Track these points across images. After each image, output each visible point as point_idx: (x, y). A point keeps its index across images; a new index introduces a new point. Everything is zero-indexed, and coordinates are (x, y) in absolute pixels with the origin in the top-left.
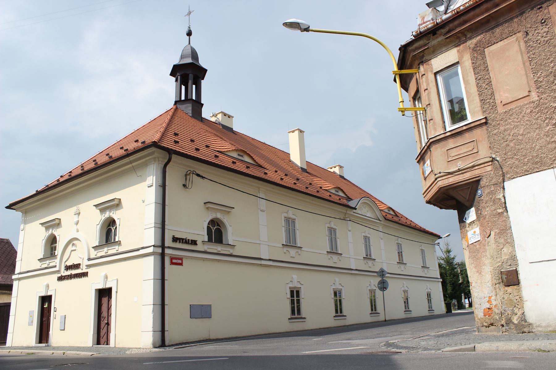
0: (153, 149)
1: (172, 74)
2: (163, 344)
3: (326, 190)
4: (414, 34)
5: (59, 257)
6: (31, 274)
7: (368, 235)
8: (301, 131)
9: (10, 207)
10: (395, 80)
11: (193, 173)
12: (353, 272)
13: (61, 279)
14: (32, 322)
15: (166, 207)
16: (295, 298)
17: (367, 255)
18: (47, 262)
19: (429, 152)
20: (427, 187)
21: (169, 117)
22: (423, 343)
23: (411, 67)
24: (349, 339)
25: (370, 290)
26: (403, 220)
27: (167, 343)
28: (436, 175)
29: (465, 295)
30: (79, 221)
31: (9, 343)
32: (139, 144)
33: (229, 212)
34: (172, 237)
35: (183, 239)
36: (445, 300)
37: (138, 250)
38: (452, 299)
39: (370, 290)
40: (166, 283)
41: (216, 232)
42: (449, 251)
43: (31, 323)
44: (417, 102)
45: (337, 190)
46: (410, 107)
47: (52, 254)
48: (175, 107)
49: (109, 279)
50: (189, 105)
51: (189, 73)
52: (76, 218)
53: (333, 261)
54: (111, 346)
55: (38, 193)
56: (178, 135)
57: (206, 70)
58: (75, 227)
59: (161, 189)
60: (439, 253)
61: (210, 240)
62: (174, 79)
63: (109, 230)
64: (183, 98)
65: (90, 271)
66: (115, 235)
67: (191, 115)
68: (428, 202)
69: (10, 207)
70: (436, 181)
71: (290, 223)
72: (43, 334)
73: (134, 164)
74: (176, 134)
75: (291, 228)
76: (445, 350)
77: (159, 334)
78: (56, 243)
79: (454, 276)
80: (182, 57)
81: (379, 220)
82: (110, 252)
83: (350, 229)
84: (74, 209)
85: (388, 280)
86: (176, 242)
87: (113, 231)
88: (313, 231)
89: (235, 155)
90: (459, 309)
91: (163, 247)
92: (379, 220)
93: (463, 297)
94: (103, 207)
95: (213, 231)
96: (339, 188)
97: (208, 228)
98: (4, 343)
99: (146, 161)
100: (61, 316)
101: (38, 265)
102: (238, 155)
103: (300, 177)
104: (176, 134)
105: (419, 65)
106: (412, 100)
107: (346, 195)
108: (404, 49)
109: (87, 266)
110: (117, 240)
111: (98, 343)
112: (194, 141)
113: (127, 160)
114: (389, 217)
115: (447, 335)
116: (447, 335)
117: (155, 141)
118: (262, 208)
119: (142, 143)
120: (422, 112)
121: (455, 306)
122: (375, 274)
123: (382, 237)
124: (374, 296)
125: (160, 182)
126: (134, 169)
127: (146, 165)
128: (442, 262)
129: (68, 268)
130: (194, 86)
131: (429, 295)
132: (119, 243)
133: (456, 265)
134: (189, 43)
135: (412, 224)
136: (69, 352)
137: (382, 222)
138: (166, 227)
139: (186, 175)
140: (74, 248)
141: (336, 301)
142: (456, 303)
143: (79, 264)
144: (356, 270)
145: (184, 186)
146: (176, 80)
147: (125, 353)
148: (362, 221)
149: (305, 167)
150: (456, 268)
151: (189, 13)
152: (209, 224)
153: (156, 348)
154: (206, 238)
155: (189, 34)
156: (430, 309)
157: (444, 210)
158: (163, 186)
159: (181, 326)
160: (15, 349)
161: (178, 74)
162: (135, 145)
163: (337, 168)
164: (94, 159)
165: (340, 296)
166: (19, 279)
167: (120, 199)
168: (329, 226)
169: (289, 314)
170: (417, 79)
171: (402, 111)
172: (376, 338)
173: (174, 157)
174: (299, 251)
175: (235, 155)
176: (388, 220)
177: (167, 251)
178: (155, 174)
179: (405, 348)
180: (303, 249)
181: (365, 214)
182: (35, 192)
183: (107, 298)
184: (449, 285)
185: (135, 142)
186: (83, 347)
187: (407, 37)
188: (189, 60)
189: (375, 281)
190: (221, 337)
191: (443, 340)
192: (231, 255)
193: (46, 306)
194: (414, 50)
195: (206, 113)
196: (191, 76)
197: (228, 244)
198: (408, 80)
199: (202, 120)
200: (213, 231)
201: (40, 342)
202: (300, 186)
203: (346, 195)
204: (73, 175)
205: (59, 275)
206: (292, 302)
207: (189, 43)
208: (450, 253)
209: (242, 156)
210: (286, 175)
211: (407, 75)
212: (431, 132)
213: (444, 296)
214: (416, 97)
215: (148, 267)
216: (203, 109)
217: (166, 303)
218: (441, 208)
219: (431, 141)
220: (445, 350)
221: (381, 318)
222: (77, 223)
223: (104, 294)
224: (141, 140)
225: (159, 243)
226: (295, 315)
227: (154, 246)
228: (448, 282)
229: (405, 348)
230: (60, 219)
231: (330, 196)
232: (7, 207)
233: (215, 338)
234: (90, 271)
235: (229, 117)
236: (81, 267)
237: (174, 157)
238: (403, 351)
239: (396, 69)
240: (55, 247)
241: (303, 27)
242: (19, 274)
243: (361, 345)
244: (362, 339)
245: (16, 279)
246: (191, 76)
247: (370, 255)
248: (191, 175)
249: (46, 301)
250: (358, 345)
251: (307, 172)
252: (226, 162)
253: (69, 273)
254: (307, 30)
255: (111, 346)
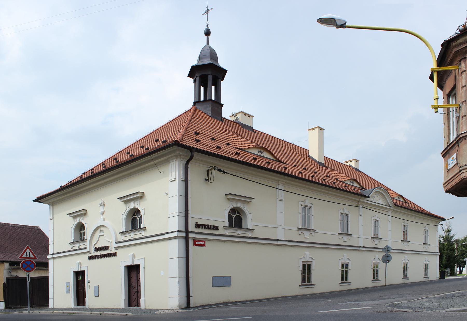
0: (175, 148)
1: (190, 75)
2: (188, 306)
3: (342, 181)
4: (461, 28)
5: (88, 241)
6: (61, 254)
7: (378, 219)
8: (321, 129)
9: (38, 200)
10: (431, 78)
11: (215, 169)
12: (361, 249)
13: (91, 258)
14: (69, 290)
15: (189, 199)
16: (307, 270)
17: (374, 235)
18: (78, 245)
19: (457, 147)
20: (449, 178)
21: (189, 118)
22: (427, 304)
23: (450, 64)
24: (357, 301)
25: (374, 263)
26: (411, 206)
27: (192, 305)
28: (461, 167)
29: (457, 265)
30: (105, 211)
31: (51, 305)
32: (160, 143)
33: (249, 202)
34: (195, 224)
35: (205, 225)
36: (440, 269)
37: (163, 234)
38: (446, 268)
39: (374, 263)
40: (191, 280)
41: (236, 218)
42: (449, 231)
43: (68, 291)
44: (451, 99)
45: (352, 181)
46: (442, 104)
47: (81, 239)
48: (194, 108)
49: (136, 258)
50: (208, 105)
51: (208, 74)
52: (101, 209)
53: (344, 240)
54: (141, 308)
55: (62, 188)
56: (199, 134)
57: (226, 71)
58: (102, 217)
59: (183, 184)
60: (441, 232)
61: (231, 225)
62: (192, 80)
63: (134, 220)
64: (202, 99)
65: (118, 251)
66: (140, 223)
67: (210, 115)
68: (447, 191)
69: (38, 200)
70: (460, 173)
71: (306, 209)
72: (80, 298)
73: (156, 161)
74: (197, 134)
75: (306, 214)
76: (449, 310)
77: (185, 300)
78: (84, 229)
79: (451, 250)
80: (201, 57)
81: (390, 206)
82: (136, 237)
83: (361, 214)
84: (99, 202)
85: (391, 254)
86: (199, 227)
87: (138, 219)
88: (327, 216)
89: (255, 152)
90: (451, 275)
91: (187, 232)
92: (390, 206)
93: (456, 267)
94: (126, 200)
95: (234, 218)
96: (355, 180)
97: (229, 215)
98: (48, 306)
99: (168, 158)
100: (95, 287)
101: (70, 247)
102: (259, 151)
103: (317, 170)
104: (197, 134)
105: (460, 61)
106: (446, 97)
107: (361, 186)
108: (447, 45)
109: (115, 248)
110: (142, 227)
111: (130, 305)
112: (215, 140)
113: (149, 158)
114: (399, 203)
115: (447, 298)
116: (447, 298)
117: (176, 141)
118: (280, 198)
119: (163, 142)
120: (454, 109)
121: (448, 273)
122: (381, 250)
123: (390, 220)
124: (377, 267)
125: (183, 177)
126: (156, 165)
127: (167, 161)
128: (442, 239)
129: (97, 249)
130: (213, 87)
131: (426, 266)
132: (145, 229)
133: (454, 241)
134: (208, 43)
135: (420, 209)
136: (104, 313)
137: (392, 208)
138: (189, 215)
139: (208, 171)
140: (101, 234)
141: (343, 271)
142: (449, 271)
143: (108, 247)
144: (364, 247)
145: (206, 180)
146: (195, 82)
147: (155, 313)
148: (375, 207)
149: (323, 162)
150: (453, 244)
151: (207, 11)
152: (229, 212)
153: (182, 309)
154: (227, 224)
155: (208, 33)
156: (426, 275)
157: (460, 198)
158: (186, 181)
159: (203, 294)
160: (57, 310)
161: (196, 75)
162: (156, 145)
163: (354, 161)
164: (114, 157)
165: (347, 268)
166: (53, 258)
167: (144, 193)
168: (342, 212)
169: (300, 282)
170: (455, 76)
171: (435, 108)
172: (380, 299)
173: (196, 155)
174: (313, 233)
175: (255, 152)
176: (398, 206)
177: (190, 235)
178: (177, 169)
179: (410, 308)
180: (316, 231)
181: (377, 202)
182: (59, 187)
183: (136, 273)
184: (445, 257)
185: (156, 141)
186: (117, 309)
187: (451, 31)
188: (207, 61)
189: (379, 256)
190: (239, 300)
191: (445, 301)
192: (250, 238)
193: (80, 279)
194: (457, 46)
195: (226, 113)
196: (210, 77)
197: (248, 229)
198: (445, 77)
199: (222, 120)
200: (234, 218)
201: (78, 305)
202: (318, 178)
203: (361, 186)
204: (95, 172)
205: (90, 255)
206: (304, 272)
207: (208, 43)
208: (450, 232)
209: (262, 153)
210: (304, 169)
211: (445, 72)
212: (462, 128)
213: (440, 266)
214: (452, 94)
215: (174, 248)
216: (223, 109)
217: (190, 275)
218: (458, 196)
219: (461, 136)
220: (449, 310)
221: (382, 283)
222: (103, 213)
223: (133, 271)
224: (161, 140)
225: (183, 229)
226: (305, 283)
227: (178, 231)
228: (444, 255)
229: (410, 308)
230: (86, 210)
231: (346, 186)
232: (34, 201)
233: (234, 301)
234: (118, 251)
235: (249, 117)
236: (110, 248)
237: (196, 155)
238: (409, 310)
239: (434, 65)
240: (84, 233)
241: (339, 23)
242: (53, 254)
243: (368, 305)
244: (368, 301)
245: (51, 258)
246: (210, 77)
247: (378, 235)
248: (213, 170)
249: (80, 276)
250: (365, 306)
251: (325, 166)
252: (244, 157)
253: (99, 253)
254: (343, 26)
255: (141, 308)
